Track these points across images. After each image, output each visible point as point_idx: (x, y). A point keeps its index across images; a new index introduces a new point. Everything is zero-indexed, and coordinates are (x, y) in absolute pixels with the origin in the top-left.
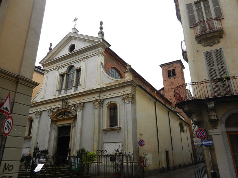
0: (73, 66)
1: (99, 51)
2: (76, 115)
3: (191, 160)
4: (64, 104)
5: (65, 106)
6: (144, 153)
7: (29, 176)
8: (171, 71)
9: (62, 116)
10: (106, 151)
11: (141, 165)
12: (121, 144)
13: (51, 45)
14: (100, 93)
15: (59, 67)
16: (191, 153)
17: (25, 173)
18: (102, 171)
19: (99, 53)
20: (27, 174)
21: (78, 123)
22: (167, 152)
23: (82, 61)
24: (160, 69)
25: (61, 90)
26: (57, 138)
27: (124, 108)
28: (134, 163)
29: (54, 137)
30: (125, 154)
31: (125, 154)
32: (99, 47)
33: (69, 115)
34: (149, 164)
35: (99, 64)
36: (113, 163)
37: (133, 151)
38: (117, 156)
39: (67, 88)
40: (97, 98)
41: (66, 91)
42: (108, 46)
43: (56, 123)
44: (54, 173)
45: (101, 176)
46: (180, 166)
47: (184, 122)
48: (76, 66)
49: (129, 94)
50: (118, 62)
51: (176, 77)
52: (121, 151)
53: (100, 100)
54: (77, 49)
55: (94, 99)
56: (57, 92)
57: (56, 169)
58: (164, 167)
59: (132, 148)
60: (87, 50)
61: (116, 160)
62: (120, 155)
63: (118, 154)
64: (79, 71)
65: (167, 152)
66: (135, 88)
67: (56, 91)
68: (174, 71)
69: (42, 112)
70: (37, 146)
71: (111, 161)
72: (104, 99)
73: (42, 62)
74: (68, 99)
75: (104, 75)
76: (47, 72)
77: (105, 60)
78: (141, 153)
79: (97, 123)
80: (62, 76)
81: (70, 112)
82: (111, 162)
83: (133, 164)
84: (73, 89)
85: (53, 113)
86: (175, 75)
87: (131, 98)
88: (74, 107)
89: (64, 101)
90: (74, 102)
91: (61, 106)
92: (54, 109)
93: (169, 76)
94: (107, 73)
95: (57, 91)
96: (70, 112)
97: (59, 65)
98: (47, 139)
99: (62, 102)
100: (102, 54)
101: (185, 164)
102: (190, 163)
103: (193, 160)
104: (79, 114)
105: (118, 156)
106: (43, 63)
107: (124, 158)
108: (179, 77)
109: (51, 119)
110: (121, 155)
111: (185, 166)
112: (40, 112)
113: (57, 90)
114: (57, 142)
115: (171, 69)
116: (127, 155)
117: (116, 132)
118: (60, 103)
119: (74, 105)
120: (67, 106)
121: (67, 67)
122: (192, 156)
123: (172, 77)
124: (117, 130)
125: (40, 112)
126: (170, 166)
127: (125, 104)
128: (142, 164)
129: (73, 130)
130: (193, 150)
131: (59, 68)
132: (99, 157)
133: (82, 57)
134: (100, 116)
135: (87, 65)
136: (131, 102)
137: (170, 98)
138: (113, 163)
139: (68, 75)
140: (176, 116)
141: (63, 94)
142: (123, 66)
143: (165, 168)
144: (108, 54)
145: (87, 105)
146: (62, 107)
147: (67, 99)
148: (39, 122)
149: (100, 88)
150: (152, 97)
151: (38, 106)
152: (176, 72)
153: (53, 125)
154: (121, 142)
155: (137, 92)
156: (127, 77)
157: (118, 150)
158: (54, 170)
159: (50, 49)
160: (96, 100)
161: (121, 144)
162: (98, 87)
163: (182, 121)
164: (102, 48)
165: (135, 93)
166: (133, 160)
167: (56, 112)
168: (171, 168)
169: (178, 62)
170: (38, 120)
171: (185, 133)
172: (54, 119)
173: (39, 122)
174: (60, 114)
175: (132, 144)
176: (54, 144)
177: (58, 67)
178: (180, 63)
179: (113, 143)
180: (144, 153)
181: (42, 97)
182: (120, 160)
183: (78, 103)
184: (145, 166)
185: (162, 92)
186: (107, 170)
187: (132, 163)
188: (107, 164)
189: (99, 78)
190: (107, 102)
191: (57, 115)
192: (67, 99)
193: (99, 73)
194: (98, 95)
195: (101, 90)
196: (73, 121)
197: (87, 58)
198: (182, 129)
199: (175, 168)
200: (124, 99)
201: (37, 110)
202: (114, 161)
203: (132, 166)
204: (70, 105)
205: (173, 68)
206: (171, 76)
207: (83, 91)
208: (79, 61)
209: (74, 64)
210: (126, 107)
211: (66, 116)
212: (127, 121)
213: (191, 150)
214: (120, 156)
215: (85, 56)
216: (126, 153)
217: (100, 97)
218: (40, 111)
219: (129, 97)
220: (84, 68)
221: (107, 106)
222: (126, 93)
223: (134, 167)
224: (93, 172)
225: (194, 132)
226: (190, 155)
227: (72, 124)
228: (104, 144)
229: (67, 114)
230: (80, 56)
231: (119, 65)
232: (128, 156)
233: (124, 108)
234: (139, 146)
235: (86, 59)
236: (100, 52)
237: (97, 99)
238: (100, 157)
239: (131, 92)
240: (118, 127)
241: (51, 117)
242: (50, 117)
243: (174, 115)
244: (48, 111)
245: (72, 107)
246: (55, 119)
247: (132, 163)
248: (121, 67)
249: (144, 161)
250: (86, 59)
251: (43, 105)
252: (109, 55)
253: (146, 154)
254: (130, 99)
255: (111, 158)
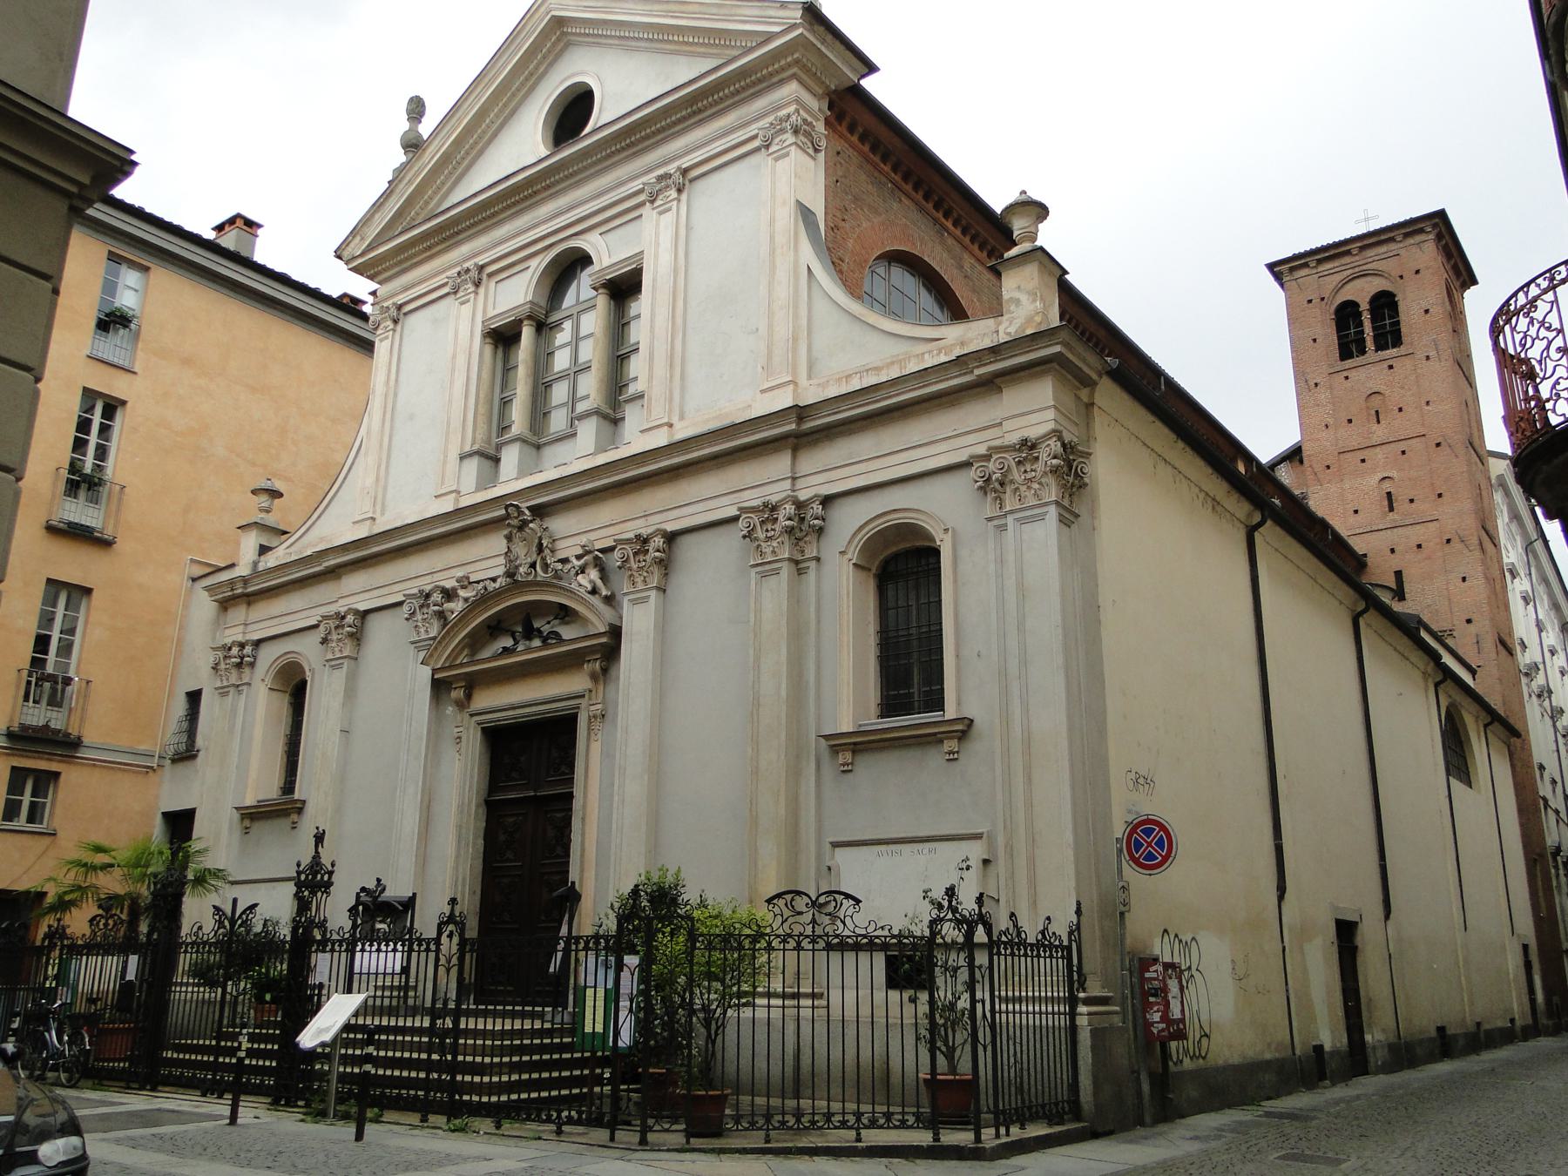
0: (583, 260)
1: (784, 112)
2: (615, 632)
3: (1526, 999)
4: (520, 549)
5: (533, 565)
6: (1166, 931)
7: (651, 1070)
8: (1364, 306)
9: (509, 642)
10: (848, 896)
11: (1148, 1025)
12: (975, 851)
13: (416, 109)
14: (795, 450)
15: (479, 277)
16: (1525, 947)
17: (232, 1052)
18: (731, 1068)
19: (782, 131)
20: (241, 1060)
21: (376, 368)
22: (1346, 931)
23: (646, 210)
24: (1275, 297)
25: (499, 447)
26: (483, 811)
27: (1001, 561)
28: (1087, 1002)
29: (461, 807)
30: (1016, 925)
31: (1016, 925)
32: (782, 82)
33: (564, 637)
34: (1204, 1017)
35: (786, 217)
36: (913, 1000)
37: (1078, 912)
38: (948, 947)
39: (537, 441)
40: (776, 493)
41: (539, 458)
42: (854, 70)
43: (469, 696)
44: (439, 1066)
45: (797, 1097)
46: (1445, 1044)
47: (1474, 707)
48: (608, 253)
49: (1033, 447)
50: (940, 215)
51: (1403, 350)
52: (980, 900)
53: (800, 505)
54: (606, 112)
55: (753, 499)
56: (473, 465)
57: (456, 1032)
58: (1327, 1047)
59: (1073, 884)
60: (684, 119)
61: (940, 981)
62: (969, 935)
63: (950, 932)
64: (623, 288)
65: (1346, 931)
66: (1084, 394)
67: (462, 458)
68: (1385, 304)
69: (372, 617)
70: (317, 856)
71: (892, 983)
72: (827, 501)
73: (357, 247)
74: (548, 515)
75: (821, 306)
76: (396, 322)
77: (835, 187)
78: (1144, 929)
79: (774, 686)
80: (503, 338)
81: (565, 614)
82: (894, 995)
83: (1082, 1009)
84: (588, 431)
85: (444, 626)
86: (1397, 342)
87: (1055, 471)
88: (594, 574)
89: (523, 525)
90: (592, 536)
91: (500, 571)
92: (449, 595)
93: (1349, 347)
94: (854, 289)
95: (470, 455)
96: (563, 607)
97: (481, 260)
98: (410, 822)
99: (509, 538)
100: (808, 135)
101: (1478, 1024)
102: (1518, 1023)
103: (1540, 996)
104: (638, 621)
105: (954, 943)
106: (370, 248)
107: (1001, 963)
108: (1432, 354)
109: (434, 671)
110: (980, 935)
111: (1480, 1039)
112: (350, 619)
113: (467, 448)
114: (481, 842)
115: (1362, 292)
116: (1031, 940)
117: (934, 759)
118: (495, 544)
119: (598, 559)
120: (546, 567)
121: (538, 264)
122: (1528, 966)
123: (1371, 354)
124: (941, 741)
125: (350, 619)
126: (1368, 1038)
127: (1003, 528)
128: (1157, 1017)
129: (596, 747)
130: (1539, 922)
131: (477, 284)
132: (792, 944)
133: (651, 178)
134: (796, 634)
135: (685, 238)
136: (1053, 510)
137: (1353, 519)
138: (913, 1000)
139: (544, 327)
140: (1417, 657)
141: (513, 477)
142: (975, 248)
143: (1334, 1053)
144: (855, 139)
145: (688, 549)
146: (510, 574)
147: (540, 511)
148: (350, 692)
149: (800, 412)
150: (1225, 486)
151: (334, 573)
152: (1403, 317)
153: (450, 710)
154: (978, 837)
155: (1100, 422)
156: (1017, 302)
157: (951, 892)
158: (442, 1043)
159: (412, 145)
160: (765, 505)
161: (975, 851)
162: (784, 400)
163: (1459, 697)
164: (801, 82)
165: (1089, 438)
166: (1075, 978)
167: (465, 616)
168: (1378, 1057)
169: (1421, 231)
170: (340, 677)
171: (1479, 792)
172: (451, 667)
173: (350, 692)
174: (495, 628)
175: (1070, 853)
176: (458, 856)
177: (468, 270)
178: (1439, 237)
179: (906, 848)
180: (1166, 931)
181: (366, 509)
182: (972, 975)
183: (628, 541)
184: (1181, 1035)
185: (1285, 475)
186: (866, 1054)
187: (1073, 1001)
188: (865, 1011)
189: (783, 331)
190: (851, 521)
191: (475, 642)
192: (540, 511)
193: (783, 292)
194: (780, 464)
195: (809, 425)
196: (594, 677)
197: (685, 180)
198: (1458, 762)
199: (1405, 1055)
200: (992, 487)
201: (332, 609)
202: (920, 986)
203: (1073, 1029)
204: (565, 561)
205: (1376, 285)
206: (1363, 352)
207: (660, 439)
208: (624, 214)
209: (591, 243)
210: (1011, 558)
211: (537, 643)
212: (1024, 663)
213: (1526, 925)
214: (969, 945)
215: (671, 168)
216: (1023, 922)
217: (794, 479)
218: (356, 612)
219: (1039, 466)
220: (666, 258)
221: (853, 555)
222: (1014, 438)
223: (1085, 1038)
224: (761, 1064)
225: (1549, 787)
226: (1513, 962)
227: (584, 702)
228: (841, 853)
229: (546, 629)
230: (632, 175)
231: (950, 241)
232: (1038, 945)
233: (1001, 561)
234: (1131, 873)
235: (680, 191)
236: (789, 116)
237: (774, 499)
238: (805, 944)
239: (1051, 426)
240: (950, 712)
241: (431, 649)
242: (422, 655)
243: (1404, 643)
244: (405, 608)
245: (582, 570)
246: (462, 665)
247: (1073, 1001)
248: (966, 256)
249: (1173, 985)
250: (680, 191)
251: (376, 564)
252: (866, 148)
253: (1186, 937)
254: (1051, 480)
255: (891, 964)
